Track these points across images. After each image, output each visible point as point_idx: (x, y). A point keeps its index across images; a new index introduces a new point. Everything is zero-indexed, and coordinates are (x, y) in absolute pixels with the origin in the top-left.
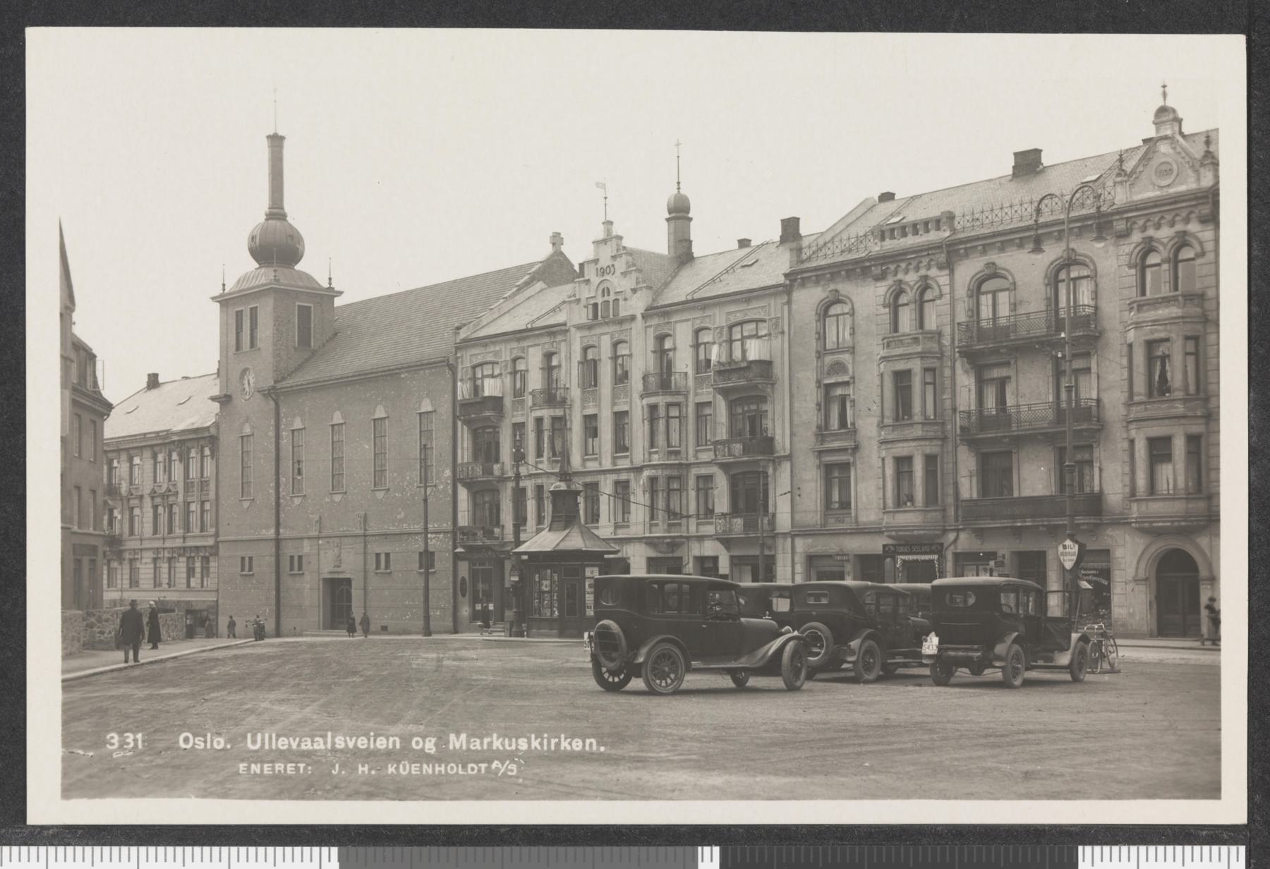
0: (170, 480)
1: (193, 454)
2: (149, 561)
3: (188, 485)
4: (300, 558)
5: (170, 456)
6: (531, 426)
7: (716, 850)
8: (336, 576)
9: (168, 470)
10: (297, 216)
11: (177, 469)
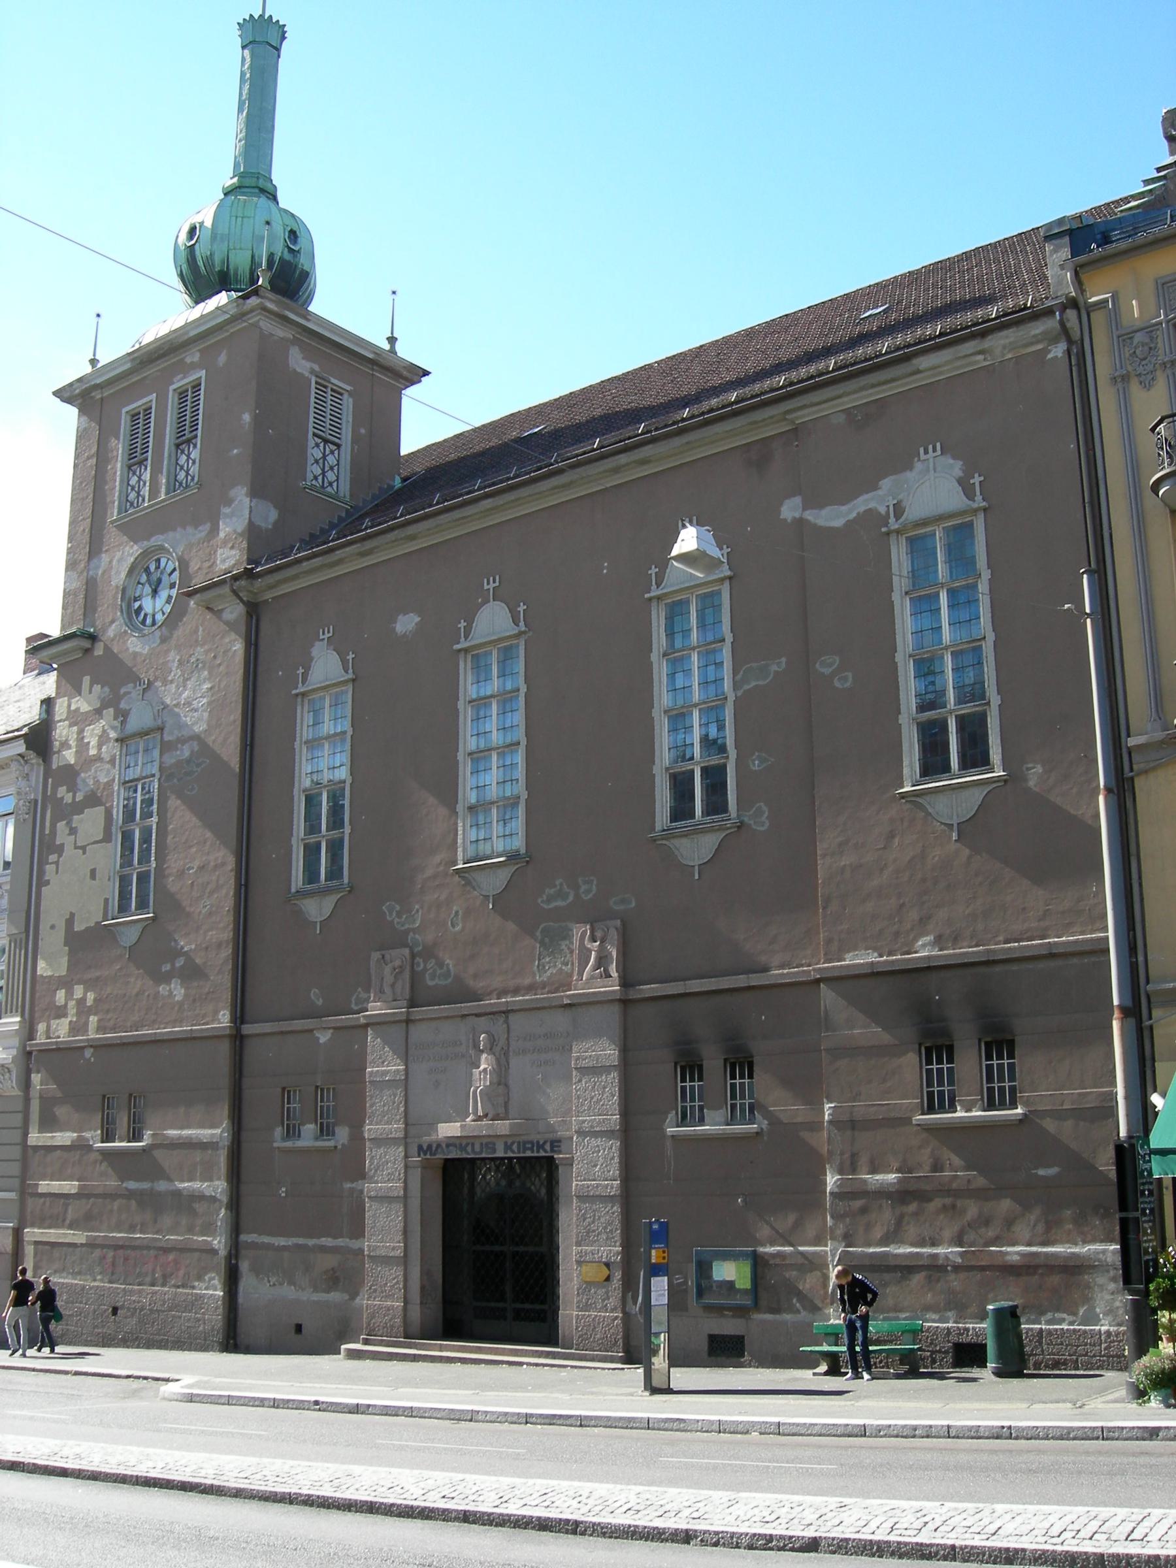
7: (417, 619)
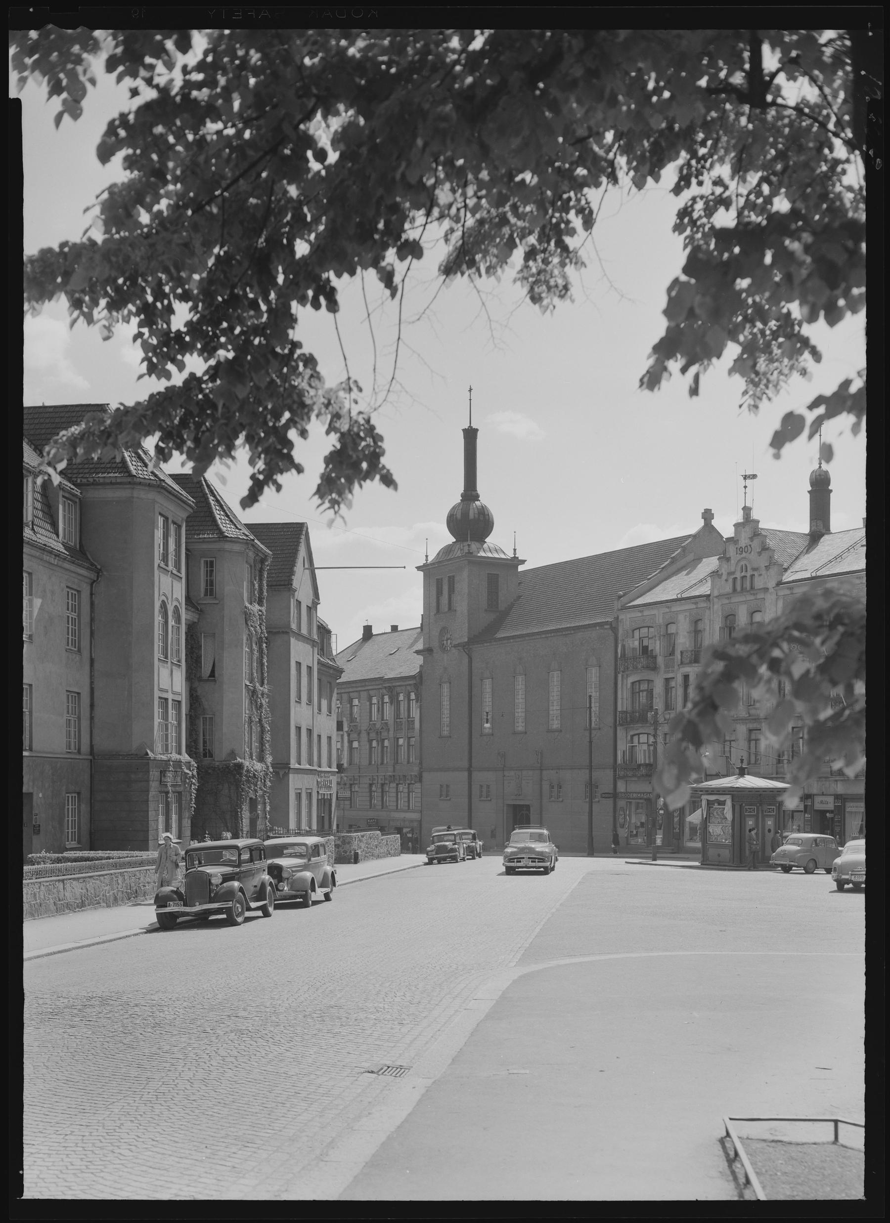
0: (383, 720)
1: (401, 697)
3: (398, 725)
4: (448, 786)
5: (383, 699)
6: (680, 679)
9: (381, 710)
10: (487, 496)
11: (403, 796)
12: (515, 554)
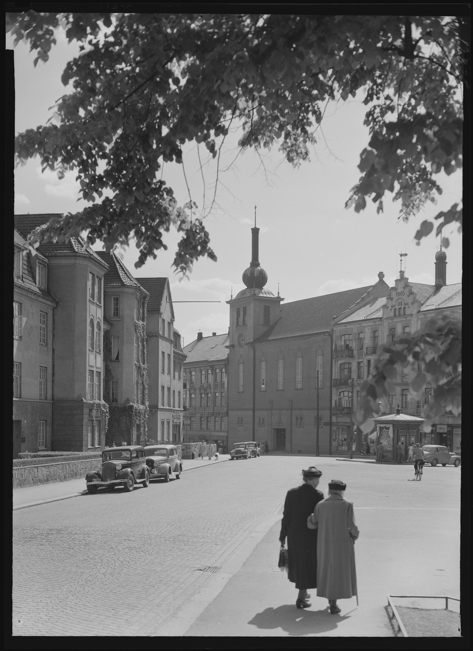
1: (218, 371)
2: (199, 418)
3: (216, 386)
6: (366, 362)
8: (279, 427)
9: (207, 378)
11: (211, 378)
12: (278, 295)
